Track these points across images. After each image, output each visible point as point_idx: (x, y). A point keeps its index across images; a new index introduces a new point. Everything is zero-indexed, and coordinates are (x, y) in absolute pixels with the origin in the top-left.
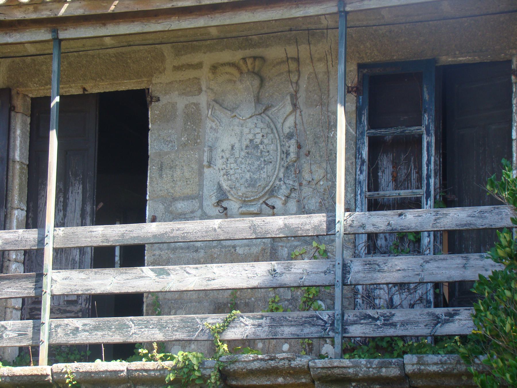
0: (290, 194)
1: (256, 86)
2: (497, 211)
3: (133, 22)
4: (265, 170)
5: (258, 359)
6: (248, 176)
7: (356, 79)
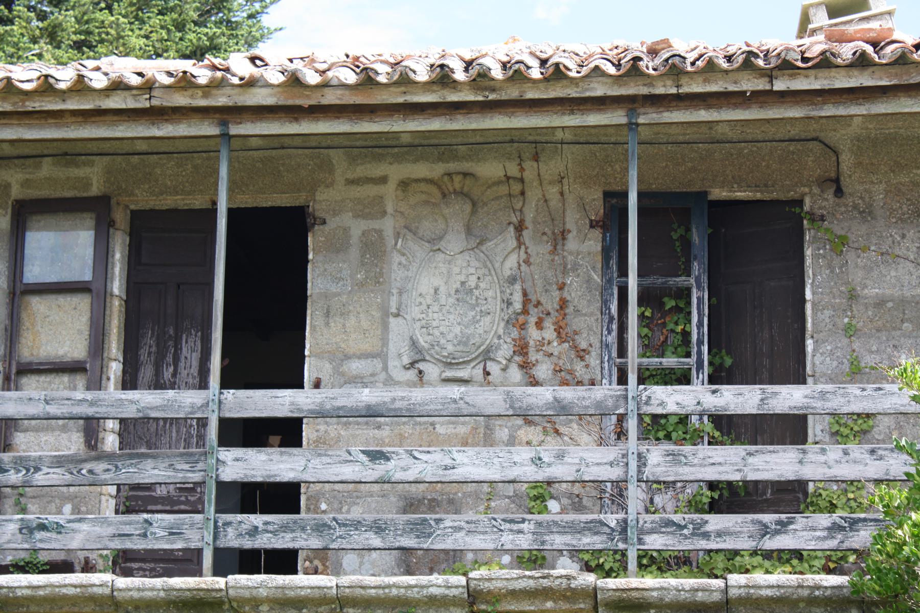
2: (842, 391)
3: (338, 118)
4: (482, 323)
5: (525, 576)
6: (457, 330)
7: (602, 211)
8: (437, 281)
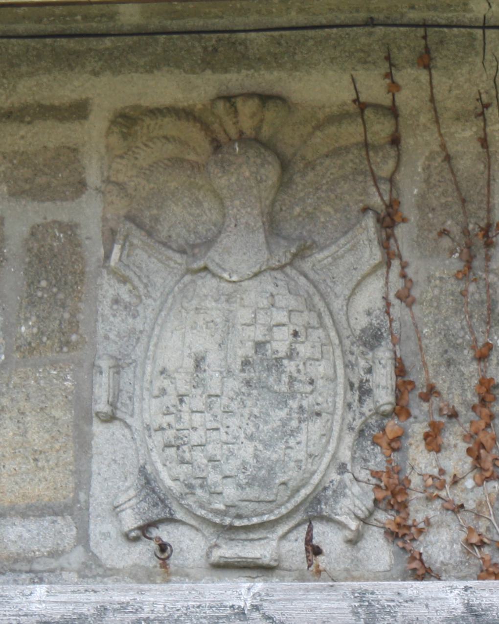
0: (371, 514)
1: (270, 183)
4: (302, 437)
6: (247, 451)
8: (202, 341)
